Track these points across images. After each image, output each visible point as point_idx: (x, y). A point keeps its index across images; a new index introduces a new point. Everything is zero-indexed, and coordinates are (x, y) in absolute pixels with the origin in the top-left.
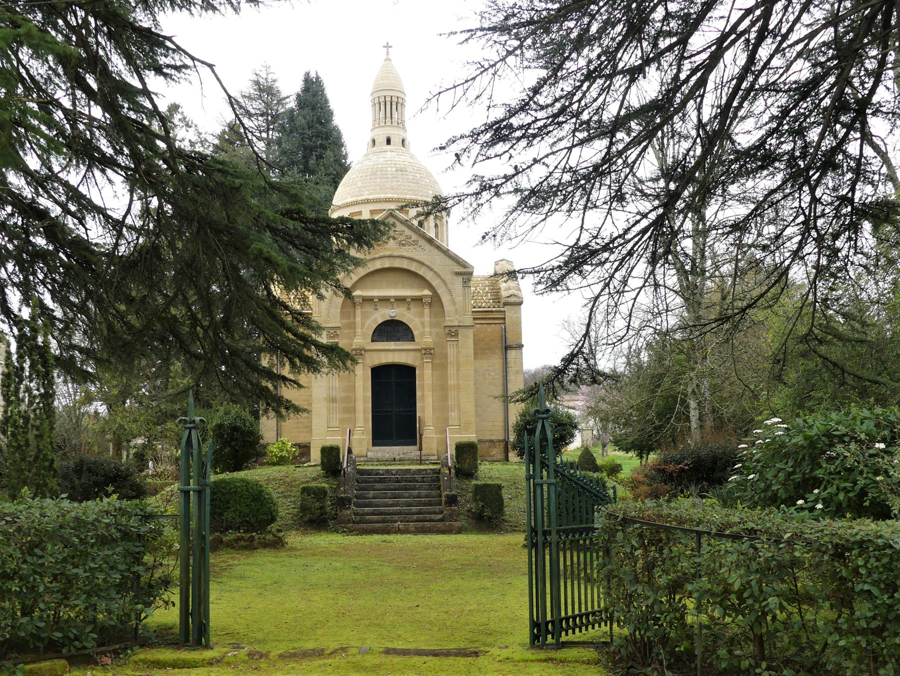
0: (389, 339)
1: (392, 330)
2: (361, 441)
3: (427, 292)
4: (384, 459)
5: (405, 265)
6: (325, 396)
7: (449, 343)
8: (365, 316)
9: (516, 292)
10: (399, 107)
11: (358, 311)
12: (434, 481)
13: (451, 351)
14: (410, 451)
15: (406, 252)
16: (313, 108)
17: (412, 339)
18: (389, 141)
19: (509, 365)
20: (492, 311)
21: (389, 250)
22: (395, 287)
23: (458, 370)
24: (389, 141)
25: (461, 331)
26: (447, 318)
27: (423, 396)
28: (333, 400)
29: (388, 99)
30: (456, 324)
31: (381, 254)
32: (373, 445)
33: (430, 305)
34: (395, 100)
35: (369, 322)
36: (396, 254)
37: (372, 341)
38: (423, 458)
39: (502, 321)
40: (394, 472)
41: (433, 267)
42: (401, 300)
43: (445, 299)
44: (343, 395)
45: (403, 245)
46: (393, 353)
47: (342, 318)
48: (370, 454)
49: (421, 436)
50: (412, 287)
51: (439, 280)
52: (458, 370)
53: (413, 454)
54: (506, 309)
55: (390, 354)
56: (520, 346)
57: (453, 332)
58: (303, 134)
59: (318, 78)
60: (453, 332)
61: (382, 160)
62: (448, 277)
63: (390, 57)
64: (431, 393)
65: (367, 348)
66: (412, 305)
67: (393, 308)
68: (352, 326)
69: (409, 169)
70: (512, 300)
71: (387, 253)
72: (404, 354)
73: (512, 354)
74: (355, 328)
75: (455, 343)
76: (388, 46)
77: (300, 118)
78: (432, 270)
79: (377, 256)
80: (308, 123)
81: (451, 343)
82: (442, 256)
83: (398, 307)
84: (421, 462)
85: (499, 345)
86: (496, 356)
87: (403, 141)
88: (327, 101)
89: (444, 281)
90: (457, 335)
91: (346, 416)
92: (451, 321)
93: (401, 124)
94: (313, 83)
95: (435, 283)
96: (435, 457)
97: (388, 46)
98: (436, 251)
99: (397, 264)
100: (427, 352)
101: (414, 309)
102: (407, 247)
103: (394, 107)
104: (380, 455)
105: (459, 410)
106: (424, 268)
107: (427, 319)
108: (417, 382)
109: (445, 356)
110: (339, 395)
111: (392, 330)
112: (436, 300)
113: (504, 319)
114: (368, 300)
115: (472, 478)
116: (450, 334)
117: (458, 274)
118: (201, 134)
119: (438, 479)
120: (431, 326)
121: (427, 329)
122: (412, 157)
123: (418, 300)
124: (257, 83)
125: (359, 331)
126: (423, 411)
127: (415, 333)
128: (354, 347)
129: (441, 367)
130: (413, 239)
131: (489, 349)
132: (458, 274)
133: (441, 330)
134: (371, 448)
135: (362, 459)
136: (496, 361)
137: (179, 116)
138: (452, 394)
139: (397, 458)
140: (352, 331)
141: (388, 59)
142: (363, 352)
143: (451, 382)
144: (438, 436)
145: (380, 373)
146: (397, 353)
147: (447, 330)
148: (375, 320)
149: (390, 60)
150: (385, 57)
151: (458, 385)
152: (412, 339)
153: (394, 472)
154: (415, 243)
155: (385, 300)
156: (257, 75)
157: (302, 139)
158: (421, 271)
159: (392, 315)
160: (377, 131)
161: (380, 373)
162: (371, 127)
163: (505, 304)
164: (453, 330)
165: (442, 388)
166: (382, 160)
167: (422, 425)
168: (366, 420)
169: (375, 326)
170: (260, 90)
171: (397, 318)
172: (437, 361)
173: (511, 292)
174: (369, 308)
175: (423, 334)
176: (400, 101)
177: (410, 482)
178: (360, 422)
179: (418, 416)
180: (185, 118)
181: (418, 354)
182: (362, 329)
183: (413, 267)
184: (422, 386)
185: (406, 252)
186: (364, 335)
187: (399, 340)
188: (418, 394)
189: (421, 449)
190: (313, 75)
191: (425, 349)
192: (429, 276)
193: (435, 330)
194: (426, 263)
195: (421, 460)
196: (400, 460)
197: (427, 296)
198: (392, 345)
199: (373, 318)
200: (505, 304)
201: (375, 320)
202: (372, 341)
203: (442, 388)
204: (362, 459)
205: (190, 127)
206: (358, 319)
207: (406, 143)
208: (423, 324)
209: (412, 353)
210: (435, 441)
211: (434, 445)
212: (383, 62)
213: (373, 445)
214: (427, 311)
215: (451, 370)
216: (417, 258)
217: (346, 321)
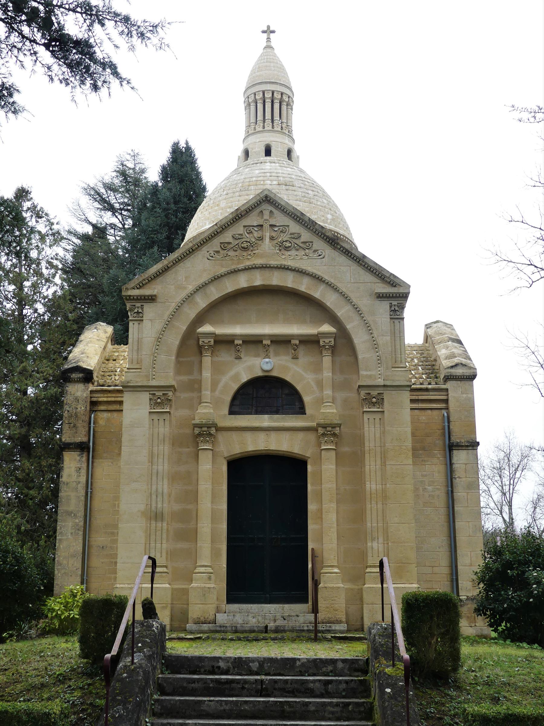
0: (259, 411)
1: (266, 395)
2: (205, 592)
3: (327, 328)
4: (247, 627)
5: (289, 281)
6: (142, 507)
7: (366, 416)
8: (217, 370)
9: (464, 361)
10: (284, 107)
11: (207, 360)
12: (353, 693)
13: (371, 430)
14: (297, 613)
15: (291, 259)
16: (181, 181)
17: (301, 410)
18: (268, 152)
19: (457, 474)
20: (427, 390)
21: (261, 256)
22: (272, 322)
23: (384, 464)
24: (268, 152)
25: (387, 396)
26: (363, 373)
27: (320, 511)
28: (157, 516)
29: (268, 95)
30: (380, 382)
31: (248, 263)
32: (230, 600)
33: (333, 349)
34: (277, 96)
35: (225, 379)
36: (273, 263)
37: (231, 412)
38: (320, 627)
39: (443, 405)
40: (255, 666)
41: (339, 285)
42: (281, 342)
43: (360, 339)
44: (177, 507)
45: (287, 249)
46: (268, 434)
47: (178, 372)
48: (221, 618)
49: (316, 584)
50: (303, 322)
51: (348, 307)
52: (384, 464)
53: (301, 619)
54: (449, 385)
55: (262, 436)
56: (474, 445)
57: (373, 398)
58: (168, 209)
59: (188, 148)
60: (373, 398)
61: (257, 172)
62: (365, 302)
63: (273, 44)
64: (334, 505)
65: (221, 424)
66: (301, 351)
67: (267, 356)
68: (195, 386)
69: (297, 184)
70: (459, 371)
71: (259, 262)
72: (286, 436)
73: (460, 457)
74: (200, 390)
75: (378, 416)
76: (269, 31)
77: (164, 190)
78: (335, 289)
79: (241, 266)
80: (174, 198)
81: (371, 416)
82: (354, 267)
83: (277, 354)
84: (315, 635)
85: (440, 443)
86: (435, 461)
87: (289, 152)
88: (198, 174)
89: (356, 309)
90: (380, 401)
91: (180, 545)
92: (370, 377)
93: (286, 130)
94: (182, 152)
95: (342, 311)
96: (343, 627)
97: (269, 31)
98: (342, 259)
99: (276, 279)
100: (328, 431)
101: (305, 357)
102: (293, 252)
103: (277, 106)
104: (239, 619)
105: (387, 539)
106: (322, 287)
107: (327, 374)
108: (309, 487)
109: (359, 440)
110: (166, 506)
111: (266, 395)
112: (342, 344)
113: (446, 401)
114: (225, 342)
115: (446, 684)
116: (368, 400)
117: (381, 297)
118: (52, 224)
119: (364, 689)
120: (335, 387)
121: (328, 392)
122: (302, 171)
123: (310, 342)
124: (123, 173)
125: (207, 394)
126: (320, 539)
127: (307, 399)
128: (197, 421)
129: (353, 460)
130: (303, 239)
131: (424, 449)
132: (381, 297)
133: (353, 395)
134: (224, 606)
135: (205, 627)
136: (435, 469)
137: (27, 205)
138: (372, 509)
139: (271, 625)
140: (195, 395)
141: (269, 47)
142: (213, 431)
143: (372, 485)
144: (349, 586)
145: (244, 471)
146: (273, 435)
147: (363, 393)
148: (236, 376)
149: (271, 47)
150: (265, 44)
151: (384, 491)
152: (301, 410)
153: (255, 666)
154: (307, 245)
155: (252, 342)
156: (123, 165)
157: (167, 216)
158: (318, 292)
159: (267, 367)
160: (252, 139)
161: (244, 471)
162: (243, 135)
163: (448, 378)
164: (374, 393)
165: (354, 498)
166: (257, 172)
167: (318, 566)
168: (215, 554)
169: (235, 387)
170: (127, 182)
171: (274, 374)
172: (346, 449)
173: (456, 360)
174: (225, 356)
175: (320, 402)
176: (285, 98)
177: (293, 693)
178: (205, 558)
179: (310, 546)
180: (35, 207)
181: (312, 437)
182: (213, 390)
183: (304, 285)
184: (319, 495)
185: (291, 259)
186: (216, 403)
187: (277, 412)
188: (312, 507)
189: (315, 610)
190: (182, 145)
191: (324, 427)
192: (330, 300)
193: (341, 396)
194: (326, 277)
195: (316, 631)
196: (277, 630)
197: (325, 335)
198: (265, 420)
199: (232, 373)
200: (448, 378)
201: (236, 376)
202: (231, 412)
203: (354, 498)
204: (205, 627)
205: (41, 217)
206: (207, 374)
207: (294, 155)
208: (320, 384)
209: (301, 435)
210: (343, 596)
211: (341, 603)
212: (261, 51)
213: (230, 600)
214: (327, 360)
215: (371, 465)
216: (310, 269)
217: (184, 378)
